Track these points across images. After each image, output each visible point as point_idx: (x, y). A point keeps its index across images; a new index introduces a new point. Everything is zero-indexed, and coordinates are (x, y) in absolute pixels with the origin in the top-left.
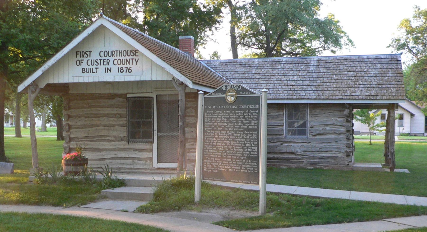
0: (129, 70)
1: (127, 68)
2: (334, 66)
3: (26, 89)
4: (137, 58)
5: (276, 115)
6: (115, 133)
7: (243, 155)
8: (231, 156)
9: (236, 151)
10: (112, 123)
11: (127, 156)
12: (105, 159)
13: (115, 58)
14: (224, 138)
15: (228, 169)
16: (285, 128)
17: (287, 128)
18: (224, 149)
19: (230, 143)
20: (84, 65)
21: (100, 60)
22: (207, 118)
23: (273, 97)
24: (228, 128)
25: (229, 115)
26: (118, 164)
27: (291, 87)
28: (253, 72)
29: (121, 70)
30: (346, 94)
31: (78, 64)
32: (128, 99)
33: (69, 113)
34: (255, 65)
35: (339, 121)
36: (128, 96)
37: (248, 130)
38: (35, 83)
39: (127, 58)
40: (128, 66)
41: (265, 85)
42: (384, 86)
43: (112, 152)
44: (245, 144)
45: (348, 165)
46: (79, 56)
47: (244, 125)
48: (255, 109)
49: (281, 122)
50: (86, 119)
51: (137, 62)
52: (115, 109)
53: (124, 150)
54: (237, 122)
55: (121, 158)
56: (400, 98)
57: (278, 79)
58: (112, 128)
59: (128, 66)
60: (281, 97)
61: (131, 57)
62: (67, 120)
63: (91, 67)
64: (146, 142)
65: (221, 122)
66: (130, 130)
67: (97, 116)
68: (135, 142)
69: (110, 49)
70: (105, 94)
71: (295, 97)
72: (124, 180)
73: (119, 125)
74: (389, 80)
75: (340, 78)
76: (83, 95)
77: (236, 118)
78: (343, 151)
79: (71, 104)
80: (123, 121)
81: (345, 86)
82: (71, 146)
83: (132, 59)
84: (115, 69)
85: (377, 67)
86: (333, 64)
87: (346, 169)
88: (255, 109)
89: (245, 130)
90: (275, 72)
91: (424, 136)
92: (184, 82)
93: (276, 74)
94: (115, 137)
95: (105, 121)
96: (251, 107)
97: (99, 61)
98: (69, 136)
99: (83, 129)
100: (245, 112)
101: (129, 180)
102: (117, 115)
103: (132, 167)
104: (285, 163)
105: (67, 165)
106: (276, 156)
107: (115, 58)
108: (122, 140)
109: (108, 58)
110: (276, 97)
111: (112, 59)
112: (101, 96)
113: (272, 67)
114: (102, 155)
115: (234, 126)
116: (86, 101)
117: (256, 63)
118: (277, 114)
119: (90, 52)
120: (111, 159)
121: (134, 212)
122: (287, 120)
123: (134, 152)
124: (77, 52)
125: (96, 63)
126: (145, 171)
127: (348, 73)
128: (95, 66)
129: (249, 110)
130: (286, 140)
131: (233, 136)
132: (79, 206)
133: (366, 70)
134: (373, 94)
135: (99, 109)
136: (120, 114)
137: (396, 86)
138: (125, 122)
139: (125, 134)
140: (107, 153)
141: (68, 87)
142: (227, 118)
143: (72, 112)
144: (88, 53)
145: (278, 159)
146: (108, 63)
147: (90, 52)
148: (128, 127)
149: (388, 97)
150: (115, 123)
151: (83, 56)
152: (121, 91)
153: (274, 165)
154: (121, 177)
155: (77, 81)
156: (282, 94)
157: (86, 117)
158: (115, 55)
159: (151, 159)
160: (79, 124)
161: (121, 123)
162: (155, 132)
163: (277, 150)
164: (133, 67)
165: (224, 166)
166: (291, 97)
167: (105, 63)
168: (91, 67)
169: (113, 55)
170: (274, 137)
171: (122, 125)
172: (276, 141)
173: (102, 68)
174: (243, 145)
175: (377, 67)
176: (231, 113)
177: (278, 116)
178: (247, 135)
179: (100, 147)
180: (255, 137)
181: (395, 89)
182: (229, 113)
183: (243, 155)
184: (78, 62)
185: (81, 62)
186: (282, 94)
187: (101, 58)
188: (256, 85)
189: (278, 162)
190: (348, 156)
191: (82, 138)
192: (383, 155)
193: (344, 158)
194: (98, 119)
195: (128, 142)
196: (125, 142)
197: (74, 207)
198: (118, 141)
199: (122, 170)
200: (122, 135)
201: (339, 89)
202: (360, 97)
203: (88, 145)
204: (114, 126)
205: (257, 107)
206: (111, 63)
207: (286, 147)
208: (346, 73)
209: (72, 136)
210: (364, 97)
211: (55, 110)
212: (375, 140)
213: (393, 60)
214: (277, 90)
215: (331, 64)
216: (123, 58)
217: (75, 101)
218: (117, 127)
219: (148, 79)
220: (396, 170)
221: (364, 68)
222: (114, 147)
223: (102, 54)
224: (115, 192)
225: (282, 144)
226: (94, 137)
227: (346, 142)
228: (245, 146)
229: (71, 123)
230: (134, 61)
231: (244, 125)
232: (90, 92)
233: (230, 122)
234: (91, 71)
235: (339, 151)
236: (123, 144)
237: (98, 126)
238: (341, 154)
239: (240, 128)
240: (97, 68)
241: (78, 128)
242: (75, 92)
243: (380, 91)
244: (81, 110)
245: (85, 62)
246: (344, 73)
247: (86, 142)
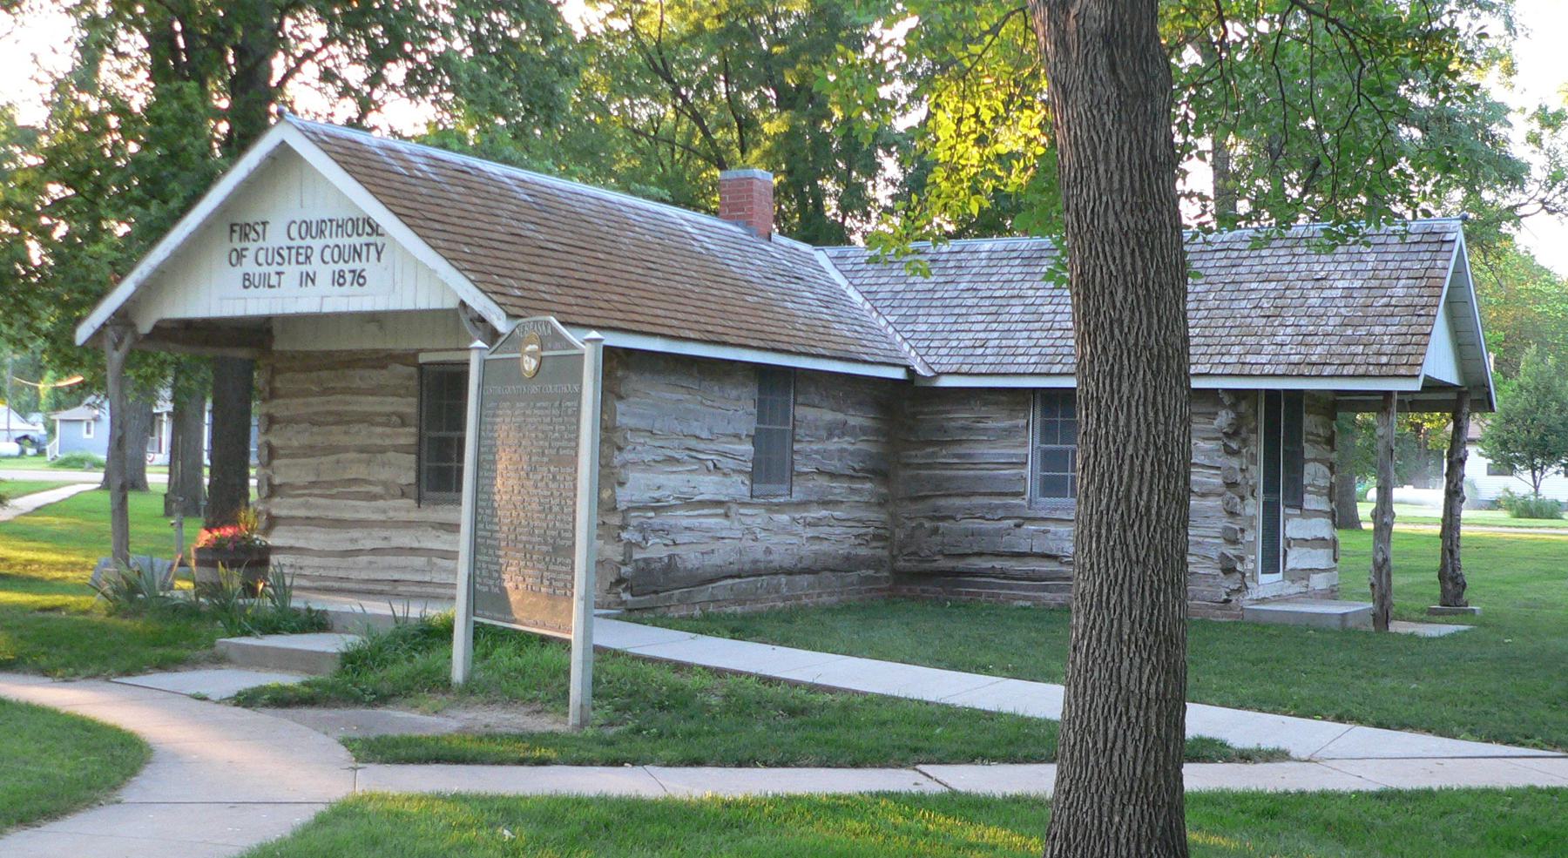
0: (359, 278)
1: (353, 271)
2: (1224, 262)
3: (99, 333)
5: (1005, 430)
11: (416, 545)
12: (359, 552)
16: (1031, 473)
17: (1039, 473)
20: (248, 265)
21: (289, 248)
23: (991, 369)
26: (390, 568)
27: (1058, 334)
28: (962, 286)
29: (339, 279)
30: (1226, 359)
32: (421, 367)
33: (272, 411)
34: (974, 263)
36: (423, 358)
38: (123, 317)
39: (356, 241)
40: (356, 265)
41: (983, 326)
42: (1363, 331)
43: (377, 532)
45: (1227, 601)
46: (236, 236)
49: (1021, 451)
50: (315, 429)
51: (379, 254)
52: (390, 399)
53: (408, 524)
55: (400, 551)
56: (1402, 371)
57: (1028, 309)
59: (356, 265)
60: (1013, 369)
61: (365, 239)
62: (267, 431)
63: (265, 269)
66: (425, 464)
67: (341, 419)
68: (436, 503)
69: (314, 216)
70: (363, 352)
71: (1056, 369)
72: (325, 612)
73: (397, 449)
74: (1388, 311)
75: (1226, 304)
76: (308, 354)
78: (1214, 555)
79: (278, 384)
80: (407, 436)
81: (1235, 331)
82: (274, 512)
83: (368, 245)
84: (324, 273)
85: (1363, 266)
86: (1223, 254)
87: (1220, 616)
90: (1028, 285)
92: (485, 314)
93: (1031, 292)
94: (384, 484)
95: (361, 435)
97: (285, 253)
98: (269, 479)
101: (338, 614)
102: (394, 418)
103: (427, 579)
104: (1026, 588)
105: (199, 563)
106: (998, 564)
108: (403, 495)
109: (309, 241)
110: (998, 369)
111: (317, 244)
112: (353, 361)
113: (1025, 270)
114: (353, 541)
116: (314, 375)
117: (983, 255)
118: (1007, 424)
119: (264, 224)
120: (374, 551)
121: (220, 702)
122: (1037, 444)
124: (232, 226)
125: (278, 259)
126: (416, 589)
127: (1261, 286)
130: (1031, 514)
132: (108, 680)
133: (1322, 274)
134: (1314, 359)
135: (348, 398)
137: (1404, 330)
139: (411, 477)
140: (365, 532)
141: (269, 331)
143: (279, 408)
144: (259, 228)
145: (1005, 574)
146: (308, 258)
147: (264, 224)
148: (419, 459)
149: (1361, 370)
150: (388, 442)
153: (993, 595)
154: (320, 602)
156: (1020, 359)
157: (313, 424)
158: (327, 233)
160: (296, 444)
161: (402, 441)
163: (1004, 544)
164: (370, 267)
166: (1044, 369)
167: (302, 259)
168: (265, 269)
170: (996, 501)
171: (403, 449)
172: (1000, 513)
175: (1363, 266)
177: (1010, 432)
179: (347, 515)
181: (1396, 339)
184: (234, 255)
185: (240, 256)
186: (1020, 359)
188: (955, 327)
189: (1002, 587)
190: (1229, 570)
192: (1434, 577)
193: (1215, 577)
194: (344, 428)
195: (419, 501)
196: (412, 502)
197: (91, 682)
198: (393, 497)
199: (401, 588)
201: (1209, 341)
202: (1268, 369)
203: (317, 507)
204: (382, 450)
206: (315, 258)
207: (1031, 536)
208: (1253, 286)
209: (277, 481)
210: (1281, 370)
211: (1459, 429)
213: (1426, 238)
214: (1012, 343)
215: (1218, 255)
216: (344, 241)
217: (289, 375)
218: (391, 455)
219: (408, 305)
220: (1397, 627)
221: (1317, 267)
222: (382, 517)
224: (265, 648)
225: (1018, 526)
226: (332, 484)
227: (1225, 522)
229: (275, 442)
230: (372, 248)
232: (325, 348)
234: (266, 282)
235: (1202, 552)
236: (404, 508)
237: (346, 449)
238: (1209, 563)
240: (279, 273)
241: (293, 456)
242: (287, 348)
243: (1344, 349)
244: (301, 400)
245: (250, 254)
246: (1245, 286)
247: (311, 500)
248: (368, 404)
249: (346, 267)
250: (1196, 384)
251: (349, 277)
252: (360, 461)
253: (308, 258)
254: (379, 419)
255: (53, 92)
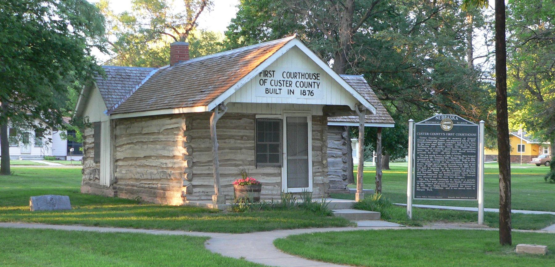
0: (311, 93)
4: (318, 82)
6: (242, 157)
7: (461, 175)
8: (449, 176)
9: (454, 172)
10: (239, 145)
13: (298, 80)
14: (441, 162)
15: (444, 188)
18: (441, 170)
19: (447, 165)
21: (284, 81)
22: (420, 143)
24: (445, 152)
25: (446, 142)
29: (303, 93)
31: (262, 83)
33: (191, 134)
35: (336, 144)
36: (257, 117)
37: (466, 154)
39: (310, 81)
40: (310, 89)
44: (463, 166)
47: (462, 150)
48: (473, 137)
52: (242, 131)
54: (454, 147)
58: (239, 151)
59: (310, 89)
61: (313, 80)
63: (274, 87)
64: (274, 166)
65: (436, 147)
68: (263, 166)
70: (231, 114)
77: (454, 144)
80: (251, 144)
83: (314, 83)
84: (298, 91)
88: (473, 137)
89: (463, 154)
91: (66, 159)
94: (242, 160)
96: (469, 135)
97: (282, 82)
99: (207, 153)
100: (462, 139)
107: (298, 80)
109: (290, 79)
111: (294, 81)
115: (451, 150)
119: (273, 71)
123: (262, 177)
128: (278, 87)
129: (467, 137)
131: (450, 159)
135: (225, 130)
136: (246, 136)
138: (253, 145)
139: (253, 158)
142: (444, 145)
144: (272, 73)
146: (290, 85)
147: (273, 71)
150: (242, 146)
151: (267, 75)
152: (250, 112)
155: (260, 102)
158: (298, 77)
159: (280, 184)
161: (249, 145)
162: (285, 156)
164: (315, 90)
165: (440, 185)
167: (288, 85)
168: (274, 87)
169: (296, 76)
173: (285, 89)
174: (461, 166)
176: (448, 139)
178: (465, 158)
179: (226, 172)
180: (473, 160)
182: (445, 140)
183: (461, 175)
185: (264, 82)
187: (284, 79)
191: (205, 163)
193: (341, 181)
194: (223, 141)
196: (254, 167)
200: (249, 159)
205: (475, 135)
212: (15, 166)
216: (305, 80)
217: (198, 121)
223: (285, 75)
228: (463, 167)
229: (193, 146)
230: (316, 84)
231: (462, 150)
233: (446, 147)
234: (275, 91)
238: (338, 177)
239: (458, 152)
240: (280, 89)
241: (201, 151)
244: (205, 130)
248: (234, 132)
249: (306, 89)
250: (329, 124)
251: (307, 93)
252: (231, 153)
253: (290, 85)
254: (237, 138)
255: (165, 12)
